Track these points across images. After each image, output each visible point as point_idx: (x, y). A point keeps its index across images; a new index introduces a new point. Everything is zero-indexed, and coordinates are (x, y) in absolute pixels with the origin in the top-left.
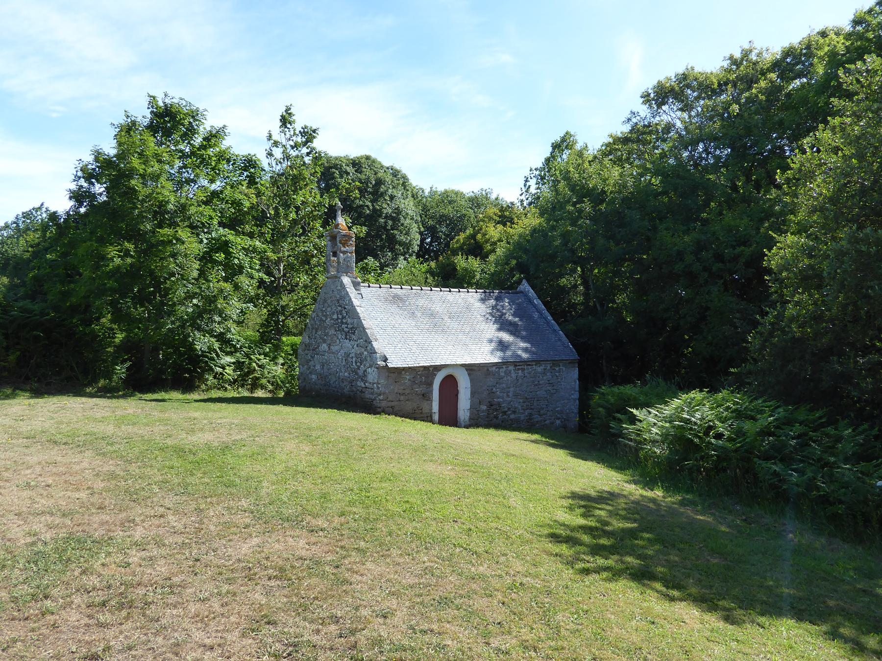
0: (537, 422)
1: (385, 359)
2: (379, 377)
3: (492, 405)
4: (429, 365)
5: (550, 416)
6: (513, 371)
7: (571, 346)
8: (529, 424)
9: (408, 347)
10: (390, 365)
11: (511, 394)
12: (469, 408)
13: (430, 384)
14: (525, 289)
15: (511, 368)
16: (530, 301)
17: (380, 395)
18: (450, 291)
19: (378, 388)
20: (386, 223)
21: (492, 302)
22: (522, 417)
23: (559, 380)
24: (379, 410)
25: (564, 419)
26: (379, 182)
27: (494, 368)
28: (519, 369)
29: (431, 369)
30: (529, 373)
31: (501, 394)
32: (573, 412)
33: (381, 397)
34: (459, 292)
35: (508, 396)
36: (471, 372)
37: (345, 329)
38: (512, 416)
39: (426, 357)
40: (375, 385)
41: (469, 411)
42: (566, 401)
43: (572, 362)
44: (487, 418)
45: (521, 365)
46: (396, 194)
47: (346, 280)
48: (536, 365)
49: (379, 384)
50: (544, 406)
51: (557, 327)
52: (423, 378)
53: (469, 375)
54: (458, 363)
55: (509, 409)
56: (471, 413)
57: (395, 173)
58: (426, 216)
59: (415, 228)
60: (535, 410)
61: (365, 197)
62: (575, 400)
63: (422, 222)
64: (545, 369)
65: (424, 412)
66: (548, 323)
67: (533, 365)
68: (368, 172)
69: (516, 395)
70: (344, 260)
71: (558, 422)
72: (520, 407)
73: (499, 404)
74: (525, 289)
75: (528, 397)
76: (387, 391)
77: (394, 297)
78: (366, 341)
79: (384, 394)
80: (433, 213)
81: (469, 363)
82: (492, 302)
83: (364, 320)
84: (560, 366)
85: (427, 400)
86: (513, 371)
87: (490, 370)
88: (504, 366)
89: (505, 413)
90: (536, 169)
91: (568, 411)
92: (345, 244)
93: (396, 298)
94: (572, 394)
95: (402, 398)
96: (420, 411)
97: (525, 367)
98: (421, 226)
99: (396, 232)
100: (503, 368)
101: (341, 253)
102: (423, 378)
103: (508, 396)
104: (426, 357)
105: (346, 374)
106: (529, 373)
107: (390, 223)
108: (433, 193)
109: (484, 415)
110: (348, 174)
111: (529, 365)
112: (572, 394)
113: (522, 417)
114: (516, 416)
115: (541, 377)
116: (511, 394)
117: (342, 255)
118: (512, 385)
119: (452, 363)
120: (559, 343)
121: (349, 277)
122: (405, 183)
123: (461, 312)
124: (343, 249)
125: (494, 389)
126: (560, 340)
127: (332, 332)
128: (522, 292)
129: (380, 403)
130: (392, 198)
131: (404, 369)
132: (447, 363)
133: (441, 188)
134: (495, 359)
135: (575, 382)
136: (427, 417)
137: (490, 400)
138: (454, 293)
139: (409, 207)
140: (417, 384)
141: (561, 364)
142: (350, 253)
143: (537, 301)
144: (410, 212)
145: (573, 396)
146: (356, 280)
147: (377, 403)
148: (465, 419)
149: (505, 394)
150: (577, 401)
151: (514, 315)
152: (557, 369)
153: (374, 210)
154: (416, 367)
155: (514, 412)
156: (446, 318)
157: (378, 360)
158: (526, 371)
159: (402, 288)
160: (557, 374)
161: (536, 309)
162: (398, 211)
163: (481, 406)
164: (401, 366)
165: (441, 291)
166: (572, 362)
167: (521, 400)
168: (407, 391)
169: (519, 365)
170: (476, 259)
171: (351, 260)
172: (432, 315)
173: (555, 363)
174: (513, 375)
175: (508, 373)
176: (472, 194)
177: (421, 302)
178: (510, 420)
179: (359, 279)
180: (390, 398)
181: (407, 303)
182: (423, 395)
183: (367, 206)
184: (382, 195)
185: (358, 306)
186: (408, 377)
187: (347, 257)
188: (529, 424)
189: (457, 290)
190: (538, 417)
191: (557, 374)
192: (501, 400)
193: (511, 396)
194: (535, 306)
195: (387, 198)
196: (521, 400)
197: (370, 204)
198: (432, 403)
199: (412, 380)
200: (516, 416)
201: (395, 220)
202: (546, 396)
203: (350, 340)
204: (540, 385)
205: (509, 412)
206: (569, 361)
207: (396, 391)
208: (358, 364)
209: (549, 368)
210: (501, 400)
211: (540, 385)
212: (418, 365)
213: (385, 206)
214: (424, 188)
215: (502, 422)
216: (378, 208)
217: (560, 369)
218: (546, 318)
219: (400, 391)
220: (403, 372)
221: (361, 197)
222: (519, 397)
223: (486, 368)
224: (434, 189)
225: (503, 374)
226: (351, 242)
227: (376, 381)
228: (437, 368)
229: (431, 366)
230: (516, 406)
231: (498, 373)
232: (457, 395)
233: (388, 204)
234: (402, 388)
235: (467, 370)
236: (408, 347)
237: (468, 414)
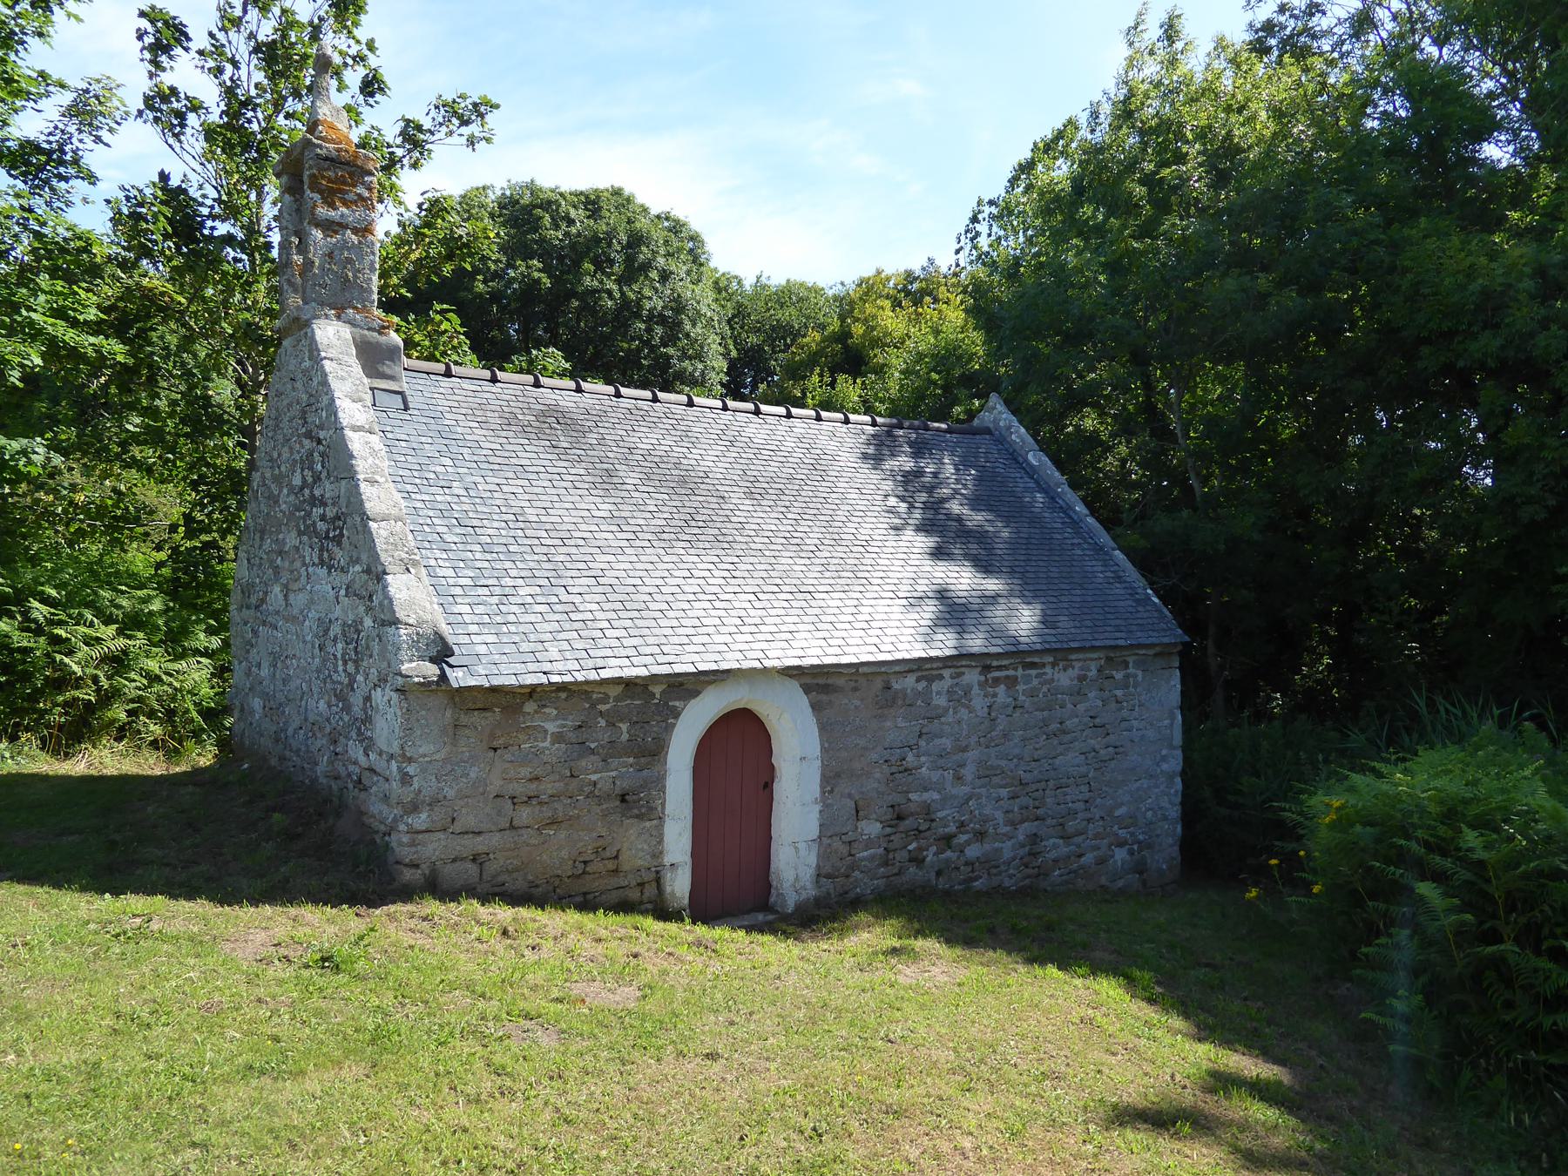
0: (1055, 861)
1: (441, 653)
2: (408, 729)
3: (900, 818)
4: (643, 672)
5: (1097, 836)
6: (976, 690)
7: (1156, 600)
8: (1030, 871)
9: (565, 597)
10: (458, 678)
11: (969, 772)
12: (815, 833)
13: (653, 752)
14: (996, 421)
15: (972, 677)
16: (1015, 458)
17: (414, 808)
18: (757, 412)
19: (406, 779)
20: (649, 330)
21: (905, 462)
22: (1007, 849)
23: (1125, 713)
24: (408, 875)
25: (1140, 843)
26: (637, 240)
27: (910, 680)
28: (997, 681)
29: (657, 690)
30: (1032, 694)
31: (935, 776)
32: (1165, 818)
33: (421, 820)
34: (789, 416)
35: (959, 778)
36: (824, 698)
37: (321, 526)
38: (973, 851)
39: (635, 641)
40: (394, 765)
41: (815, 847)
42: (1145, 783)
43: (1163, 652)
44: (886, 864)
45: (1006, 667)
46: (673, 268)
47: (332, 335)
48: (1054, 665)
49: (410, 760)
50: (1080, 806)
51: (1104, 538)
52: (624, 727)
53: (816, 707)
54: (768, 664)
55: (962, 825)
56: (824, 856)
57: (677, 227)
58: (742, 328)
59: (713, 346)
60: (1049, 821)
61: (603, 273)
62: (1171, 777)
63: (735, 339)
64: (1082, 678)
65: (626, 867)
66: (1075, 524)
67: (1044, 665)
68: (611, 218)
69: (986, 774)
70: (330, 255)
71: (1121, 855)
72: (999, 815)
73: (927, 811)
74: (996, 421)
75: (1027, 777)
76: (450, 793)
77: (542, 416)
78: (368, 571)
79: (434, 802)
80: (758, 322)
81: (816, 661)
82: (905, 462)
83: (373, 482)
84: (1127, 667)
85: (640, 817)
86: (976, 690)
87: (896, 686)
88: (946, 673)
89: (947, 840)
90: (991, 203)
91: (1149, 814)
92: (332, 192)
93: (552, 418)
94: (1164, 759)
95: (524, 815)
96: (611, 865)
97: (1020, 672)
98: (731, 347)
99: (671, 351)
100: (941, 677)
101: (317, 226)
102: (624, 727)
103: (959, 778)
104: (635, 641)
105: (322, 705)
106: (1032, 694)
107: (659, 330)
108: (760, 286)
109: (872, 858)
110: (571, 222)
111: (1033, 665)
112: (1164, 759)
113: (1007, 849)
114: (987, 847)
115: (1070, 706)
116: (969, 772)
117: (318, 234)
118: (974, 739)
119: (746, 665)
120: (1118, 589)
121: (352, 323)
122: (696, 258)
123: (791, 479)
124: (323, 211)
125: (910, 758)
126: (1119, 579)
127: (291, 539)
128: (987, 431)
129: (413, 844)
130: (665, 276)
131: (532, 692)
132: (725, 666)
133: (777, 279)
134: (944, 645)
135: (1173, 718)
136: (641, 885)
137: (898, 799)
138: (770, 419)
139: (703, 299)
140: (593, 752)
141: (1131, 660)
142: (355, 231)
143: (1035, 458)
144: (704, 310)
145: (1165, 766)
146: (383, 339)
147: (400, 844)
148: (797, 879)
149: (949, 775)
150: (1178, 780)
151: (975, 503)
152: (1119, 675)
153: (625, 303)
154: (587, 682)
155: (980, 835)
156: (736, 498)
157: (403, 654)
158: (1020, 687)
159: (579, 390)
160: (1119, 693)
161: (1037, 482)
162: (678, 306)
163: (862, 824)
164: (512, 681)
165: (725, 408)
166: (1163, 652)
167: (1004, 792)
168: (548, 787)
169: (999, 668)
170: (855, 382)
171: (361, 258)
172: (685, 483)
173: (1114, 656)
174: (979, 703)
175: (960, 697)
176: (840, 287)
177: (645, 439)
178: (967, 864)
179: (393, 335)
180: (468, 820)
181: (592, 438)
182: (623, 798)
183: (610, 293)
184: (646, 267)
185: (356, 429)
186: (551, 727)
187: (344, 245)
188: (1030, 871)
189: (781, 410)
190: (1055, 846)
191: (1119, 693)
192: (936, 796)
193: (969, 777)
194: (1031, 472)
195: (654, 275)
196: (1004, 792)
197: (615, 287)
198: (660, 827)
199: (572, 736)
200: (987, 847)
201: (673, 329)
202: (1083, 769)
203: (330, 568)
204: (1064, 732)
205: (963, 838)
206: (1158, 649)
207: (493, 789)
208: (351, 667)
209: (1093, 673)
210: (936, 796)
211: (1064, 732)
212: (593, 676)
213: (647, 292)
214: (742, 276)
215: (939, 873)
216: (632, 296)
217: (1127, 676)
218: (1066, 510)
219: (519, 789)
220: (530, 707)
221: (595, 272)
222: (996, 780)
223: (878, 683)
224: (764, 280)
225: (941, 701)
226: (360, 190)
227: (395, 749)
228: (685, 686)
229: (654, 678)
230: (987, 811)
231: (926, 696)
232: (768, 786)
233: (656, 290)
234: (525, 772)
235: (807, 689)
236: (565, 597)
237: (812, 860)
